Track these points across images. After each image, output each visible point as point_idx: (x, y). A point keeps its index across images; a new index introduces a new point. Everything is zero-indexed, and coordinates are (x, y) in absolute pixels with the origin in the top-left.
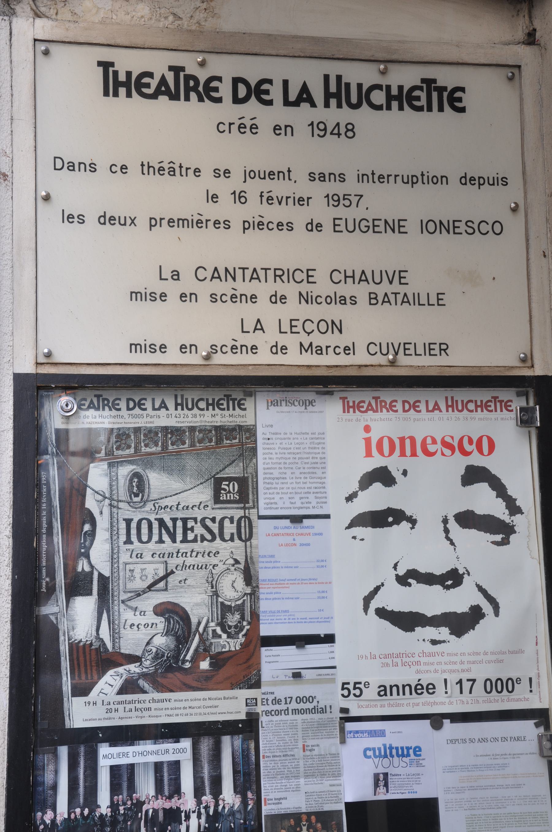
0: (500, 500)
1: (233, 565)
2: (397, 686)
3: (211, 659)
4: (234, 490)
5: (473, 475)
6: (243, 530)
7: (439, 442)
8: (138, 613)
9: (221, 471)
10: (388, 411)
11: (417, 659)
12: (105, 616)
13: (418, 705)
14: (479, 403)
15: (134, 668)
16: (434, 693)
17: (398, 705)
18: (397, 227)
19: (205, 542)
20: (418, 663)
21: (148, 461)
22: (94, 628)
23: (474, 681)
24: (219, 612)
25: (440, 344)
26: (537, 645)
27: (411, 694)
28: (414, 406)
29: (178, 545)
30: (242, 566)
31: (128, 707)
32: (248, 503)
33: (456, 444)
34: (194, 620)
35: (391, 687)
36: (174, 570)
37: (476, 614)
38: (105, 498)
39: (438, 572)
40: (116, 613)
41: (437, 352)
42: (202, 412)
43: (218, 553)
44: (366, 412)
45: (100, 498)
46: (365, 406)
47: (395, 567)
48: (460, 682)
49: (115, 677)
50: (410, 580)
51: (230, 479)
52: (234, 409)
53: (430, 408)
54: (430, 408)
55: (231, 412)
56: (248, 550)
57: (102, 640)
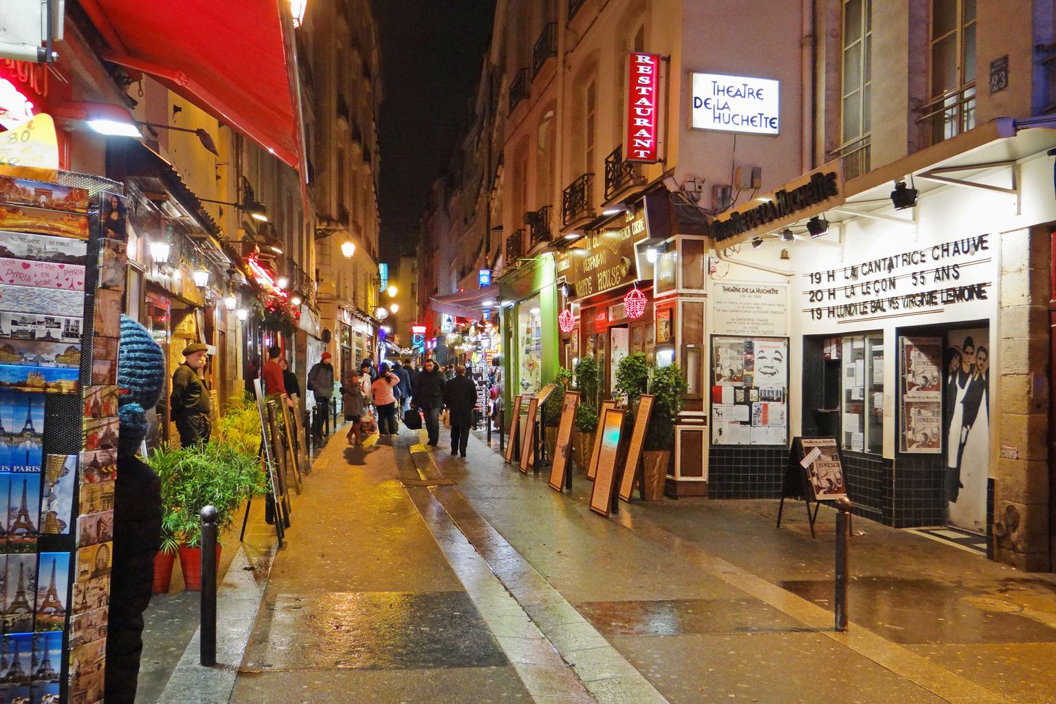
5: (777, 352)
18: (767, 312)
21: (921, 408)
44: (734, 96)
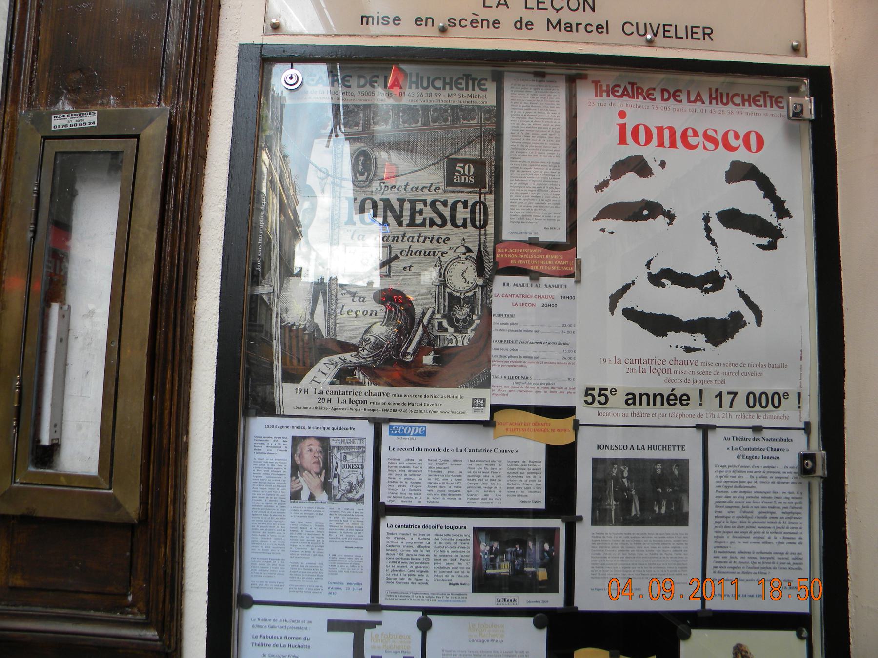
0: (768, 201)
1: (464, 254)
2: (648, 395)
3: (435, 354)
4: (469, 173)
5: (741, 172)
6: (477, 216)
7: (701, 133)
8: (356, 299)
9: (455, 152)
10: (645, 99)
11: (667, 366)
12: (321, 299)
13: (664, 416)
14: (746, 97)
15: (349, 357)
16: (688, 404)
17: (642, 415)
19: (435, 227)
20: (668, 371)
22: (309, 311)
23: (735, 394)
24: (447, 304)
25: (704, 28)
26: (784, 366)
27: (662, 404)
28: (675, 95)
29: (404, 228)
30: (474, 255)
31: (342, 398)
32: (485, 188)
33: (719, 138)
34: (418, 311)
35: (641, 396)
36: (399, 255)
37: (735, 322)
38: (328, 175)
39: (696, 274)
40: (334, 298)
41: (700, 35)
42: (438, 92)
43: (449, 239)
44: (621, 96)
45: (323, 175)
46: (621, 90)
47: (648, 265)
48: (720, 395)
49: (329, 366)
50: (664, 280)
51: (465, 161)
52: (473, 89)
53: (692, 99)
54: (692, 99)
55: (470, 92)
56: (482, 239)
57: (317, 325)
